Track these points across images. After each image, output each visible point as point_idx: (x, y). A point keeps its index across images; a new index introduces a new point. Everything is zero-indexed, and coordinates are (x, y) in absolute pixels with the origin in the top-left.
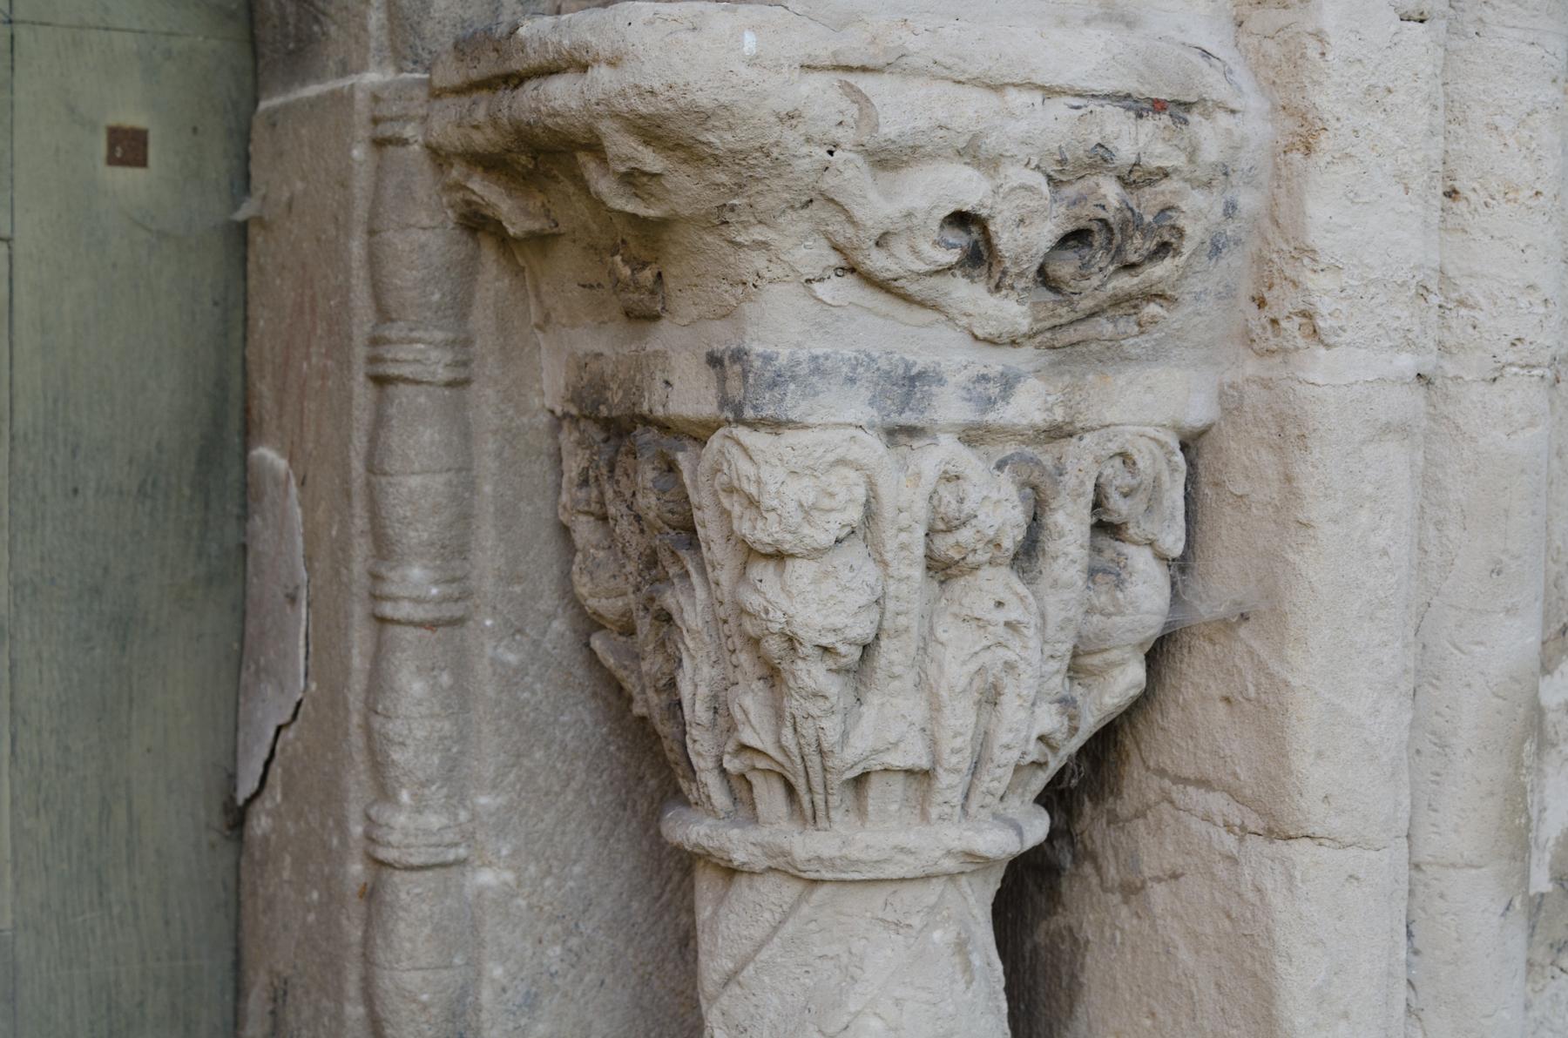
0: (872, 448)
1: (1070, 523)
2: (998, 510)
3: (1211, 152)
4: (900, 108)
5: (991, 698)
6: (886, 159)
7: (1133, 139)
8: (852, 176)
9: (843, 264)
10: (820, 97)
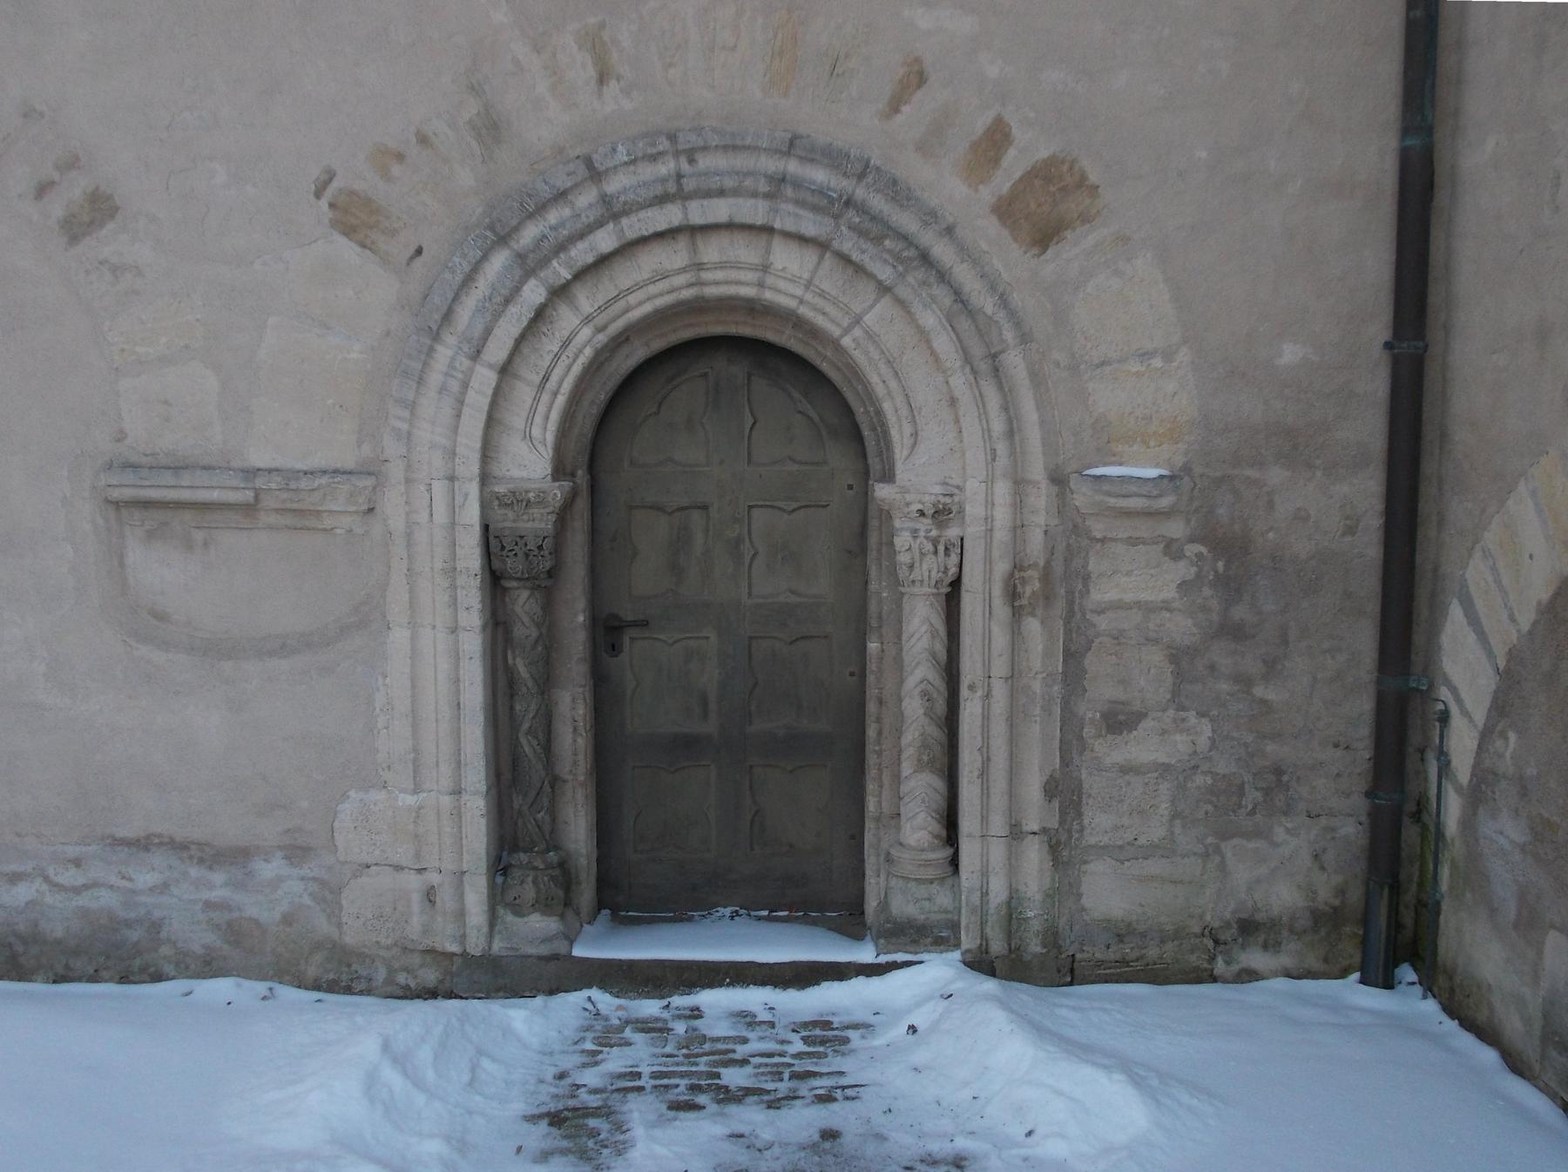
10: (898, 497)
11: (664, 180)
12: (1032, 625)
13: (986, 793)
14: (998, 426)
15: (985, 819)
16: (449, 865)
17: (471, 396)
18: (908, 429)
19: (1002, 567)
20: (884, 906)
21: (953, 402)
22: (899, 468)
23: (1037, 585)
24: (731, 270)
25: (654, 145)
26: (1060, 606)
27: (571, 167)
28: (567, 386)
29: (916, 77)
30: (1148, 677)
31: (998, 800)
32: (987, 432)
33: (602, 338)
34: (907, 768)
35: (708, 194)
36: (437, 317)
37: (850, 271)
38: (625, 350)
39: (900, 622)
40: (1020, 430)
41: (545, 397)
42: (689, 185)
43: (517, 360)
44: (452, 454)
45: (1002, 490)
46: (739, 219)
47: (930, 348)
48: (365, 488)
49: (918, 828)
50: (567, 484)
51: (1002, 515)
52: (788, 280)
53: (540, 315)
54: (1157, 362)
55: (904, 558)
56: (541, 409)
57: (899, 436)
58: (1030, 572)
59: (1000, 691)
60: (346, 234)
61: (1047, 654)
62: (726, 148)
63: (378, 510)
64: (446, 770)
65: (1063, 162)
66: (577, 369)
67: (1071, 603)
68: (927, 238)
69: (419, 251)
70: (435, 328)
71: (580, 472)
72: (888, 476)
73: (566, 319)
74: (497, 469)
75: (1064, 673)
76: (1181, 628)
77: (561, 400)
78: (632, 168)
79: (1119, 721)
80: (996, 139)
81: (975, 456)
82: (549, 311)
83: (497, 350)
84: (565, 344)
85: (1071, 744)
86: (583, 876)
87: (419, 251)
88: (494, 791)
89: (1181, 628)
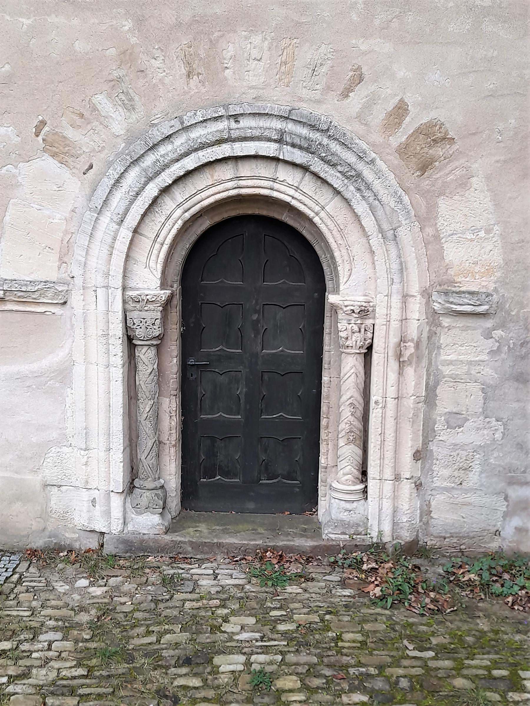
0: (347, 325)
1: (363, 330)
2: (356, 328)
3: (371, 305)
4: (346, 303)
5: (356, 342)
6: (346, 306)
7: (364, 304)
8: (343, 307)
9: (520, 588)
10: (341, 302)
11: (222, 131)
12: (410, 371)
13: (382, 458)
14: (395, 266)
15: (381, 467)
16: (103, 487)
17: (117, 245)
18: (347, 267)
19: (394, 340)
20: (328, 512)
21: (372, 252)
22: (342, 287)
23: (412, 350)
24: (255, 181)
25: (216, 112)
26: (424, 363)
27: (172, 123)
28: (169, 241)
29: (359, 78)
30: (472, 399)
31: (389, 454)
32: (389, 271)
33: (187, 215)
34: (341, 443)
35: (245, 139)
36: (101, 202)
37: (319, 183)
38: (200, 221)
39: (340, 366)
40: (407, 269)
41: (157, 246)
42: (235, 134)
43: (143, 225)
44: (107, 275)
45: (396, 300)
46: (261, 153)
47: (361, 224)
48: (61, 291)
49: (348, 469)
50: (168, 292)
51: (395, 314)
52: (287, 187)
53: (155, 201)
54: (482, 234)
55: (343, 334)
56: (155, 252)
57: (343, 270)
58: (409, 344)
59: (391, 404)
60: (53, 156)
61: (417, 385)
62: (254, 114)
63: (68, 303)
64: (102, 438)
65: (435, 126)
66: (174, 231)
67: (430, 363)
68: (360, 166)
69: (91, 167)
70: (99, 208)
71: (175, 286)
72: (336, 290)
73: (168, 204)
74: (131, 283)
75: (426, 397)
76: (489, 373)
77: (165, 248)
78: (205, 124)
79: (456, 420)
80: (401, 111)
81: (383, 283)
82: (159, 201)
83: (133, 219)
84: (169, 217)
85: (428, 433)
86: (271, 658)
87: (91, 167)
88: (128, 449)
89: (489, 373)
